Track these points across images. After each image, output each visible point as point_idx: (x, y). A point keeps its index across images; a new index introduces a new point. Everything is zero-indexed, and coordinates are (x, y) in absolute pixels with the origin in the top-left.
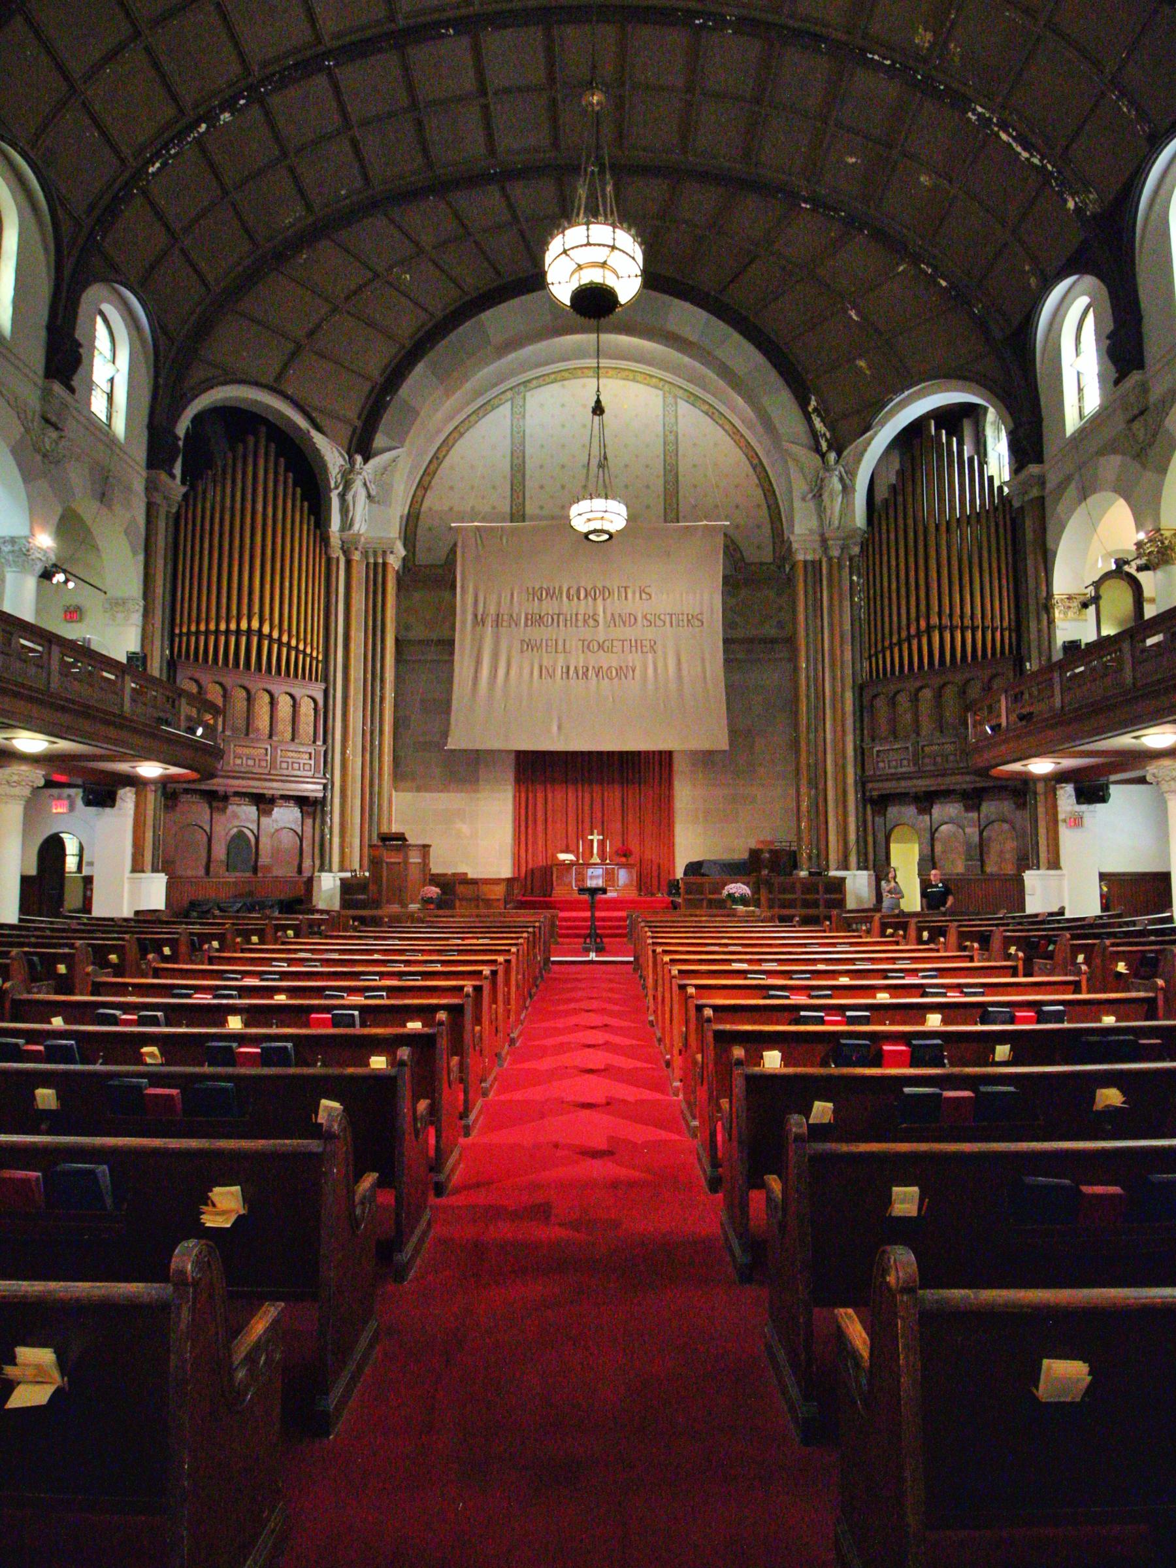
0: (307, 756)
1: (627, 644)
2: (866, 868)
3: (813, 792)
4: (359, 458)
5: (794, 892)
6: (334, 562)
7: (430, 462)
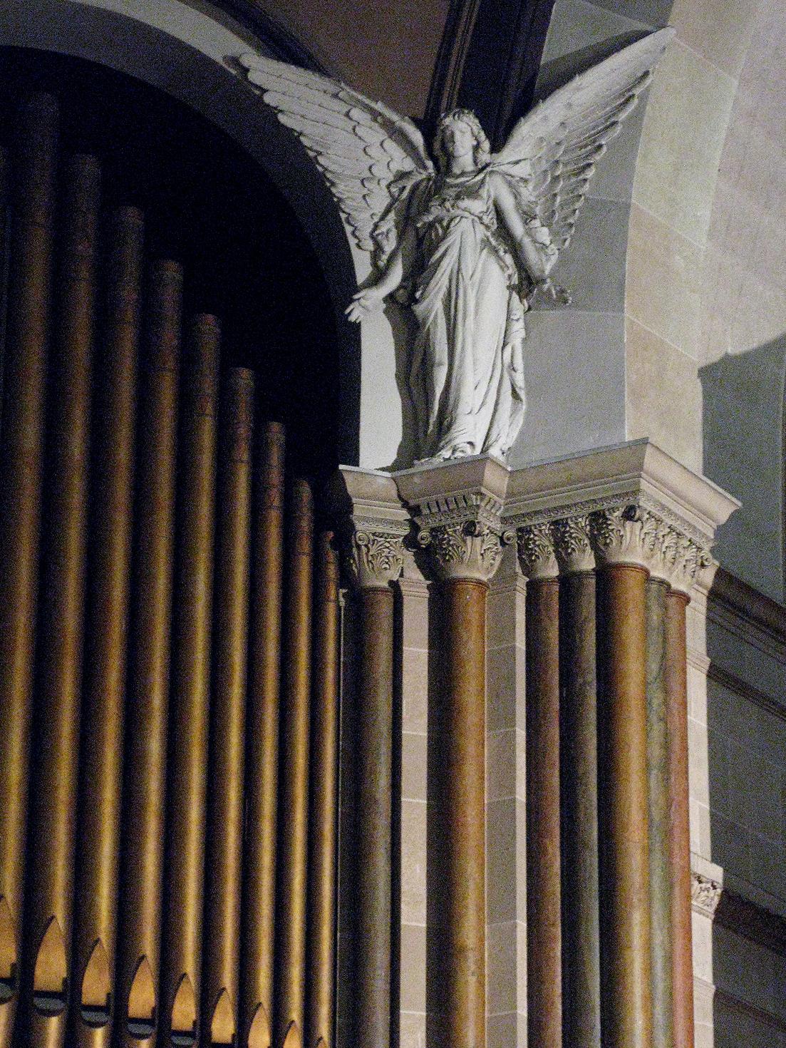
4: (465, 131)
6: (384, 608)
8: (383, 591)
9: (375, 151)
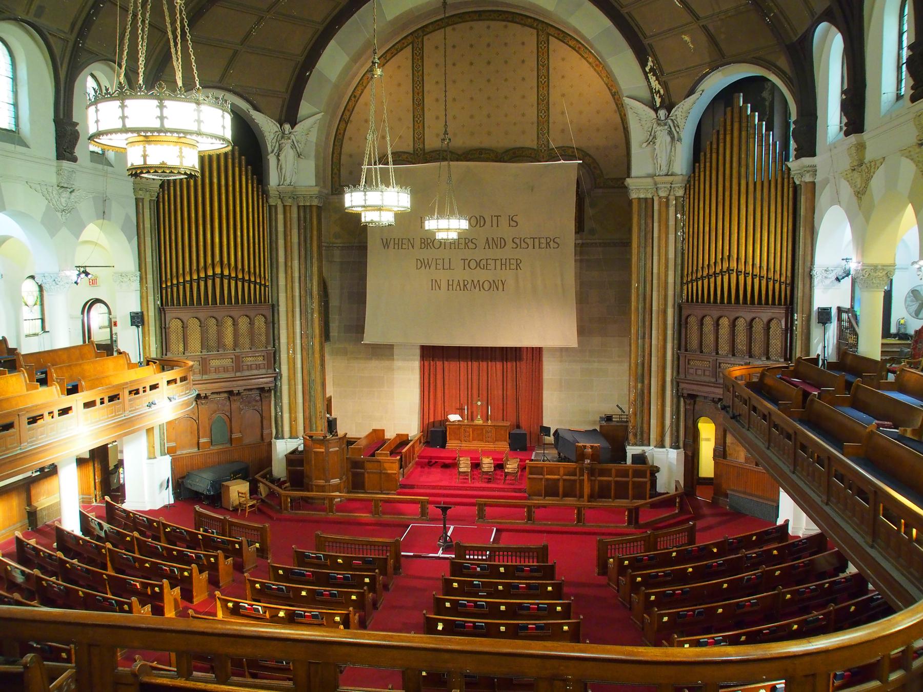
0: (261, 358)
1: (498, 262)
2: (677, 448)
3: (639, 385)
4: (287, 127)
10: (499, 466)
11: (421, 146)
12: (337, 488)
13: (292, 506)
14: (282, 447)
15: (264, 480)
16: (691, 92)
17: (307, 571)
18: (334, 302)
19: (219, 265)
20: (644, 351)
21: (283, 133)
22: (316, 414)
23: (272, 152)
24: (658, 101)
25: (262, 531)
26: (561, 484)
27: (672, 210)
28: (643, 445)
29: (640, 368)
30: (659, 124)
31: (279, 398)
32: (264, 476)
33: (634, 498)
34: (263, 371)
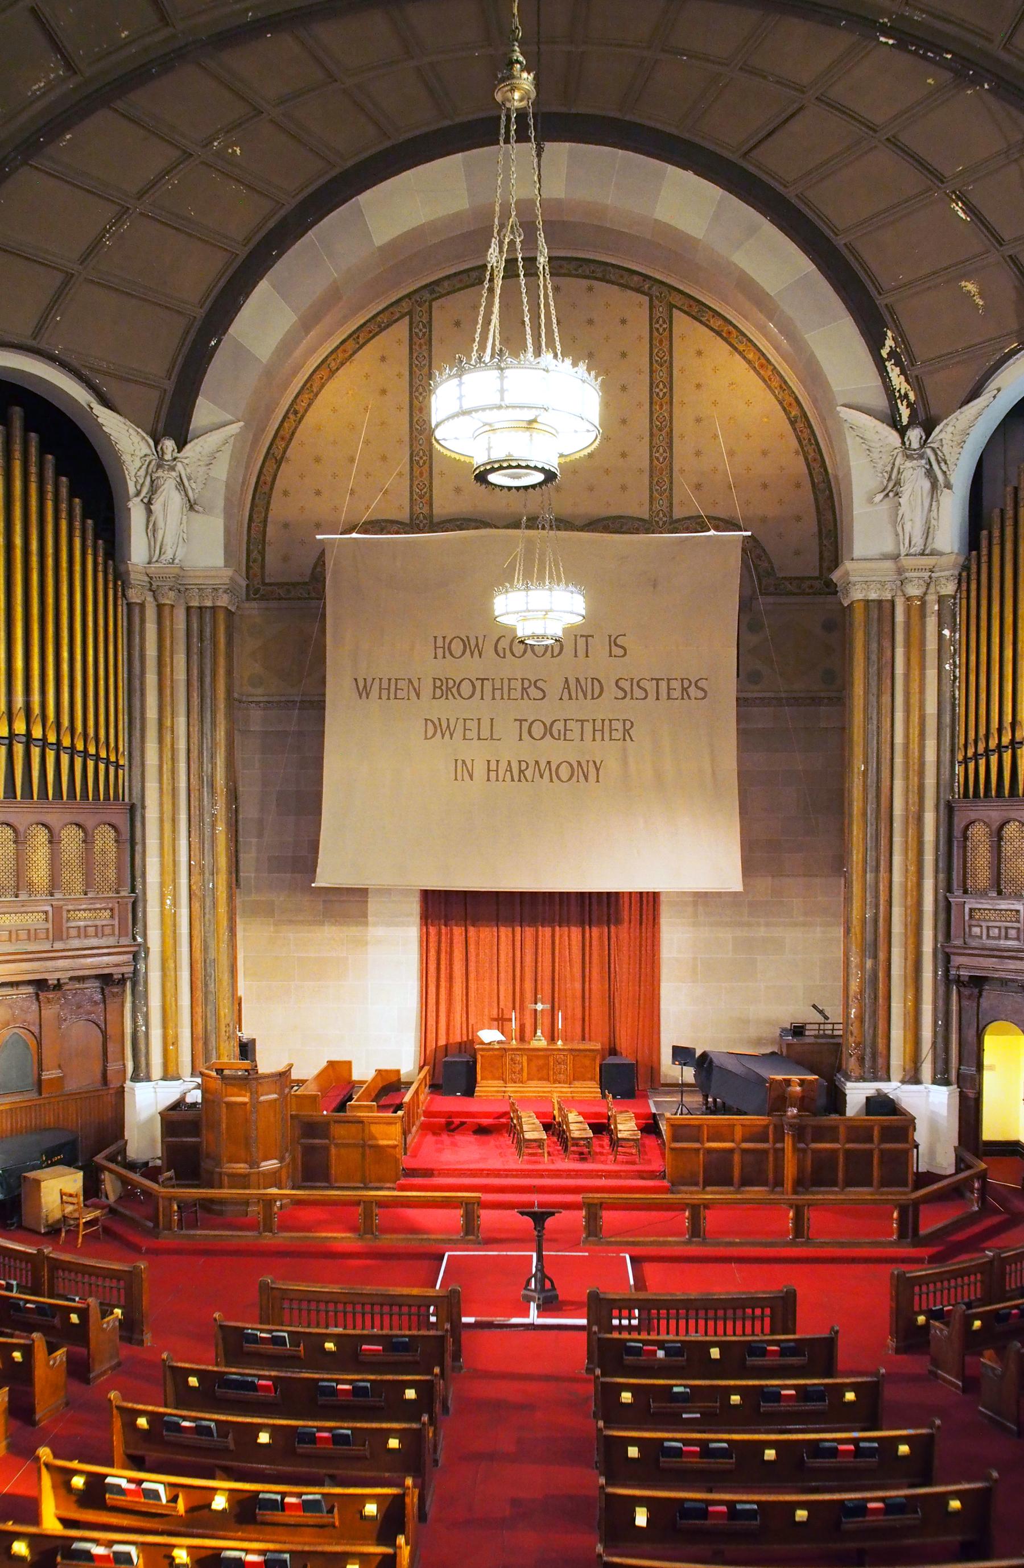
0: (107, 914)
1: (588, 727)
2: (946, 1083)
3: (869, 963)
4: (169, 444)
5: (836, 1140)
7: (286, 417)
8: (431, 1101)
9: (136, 444)
10: (601, 1127)
11: (426, 510)
12: (274, 1179)
13: (180, 1220)
14: (147, 1101)
15: (112, 1166)
16: (975, 394)
17: (263, 1376)
18: (249, 811)
19: (22, 715)
20: (877, 897)
21: (161, 457)
22: (217, 1029)
23: (138, 494)
24: (905, 413)
25: (129, 1281)
26: (737, 1158)
27: (932, 622)
28: (875, 1079)
29: (869, 928)
30: (909, 457)
31: (140, 998)
32: (112, 1159)
33: (885, 1183)
34: (111, 941)
